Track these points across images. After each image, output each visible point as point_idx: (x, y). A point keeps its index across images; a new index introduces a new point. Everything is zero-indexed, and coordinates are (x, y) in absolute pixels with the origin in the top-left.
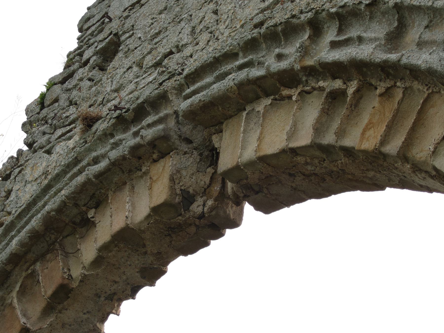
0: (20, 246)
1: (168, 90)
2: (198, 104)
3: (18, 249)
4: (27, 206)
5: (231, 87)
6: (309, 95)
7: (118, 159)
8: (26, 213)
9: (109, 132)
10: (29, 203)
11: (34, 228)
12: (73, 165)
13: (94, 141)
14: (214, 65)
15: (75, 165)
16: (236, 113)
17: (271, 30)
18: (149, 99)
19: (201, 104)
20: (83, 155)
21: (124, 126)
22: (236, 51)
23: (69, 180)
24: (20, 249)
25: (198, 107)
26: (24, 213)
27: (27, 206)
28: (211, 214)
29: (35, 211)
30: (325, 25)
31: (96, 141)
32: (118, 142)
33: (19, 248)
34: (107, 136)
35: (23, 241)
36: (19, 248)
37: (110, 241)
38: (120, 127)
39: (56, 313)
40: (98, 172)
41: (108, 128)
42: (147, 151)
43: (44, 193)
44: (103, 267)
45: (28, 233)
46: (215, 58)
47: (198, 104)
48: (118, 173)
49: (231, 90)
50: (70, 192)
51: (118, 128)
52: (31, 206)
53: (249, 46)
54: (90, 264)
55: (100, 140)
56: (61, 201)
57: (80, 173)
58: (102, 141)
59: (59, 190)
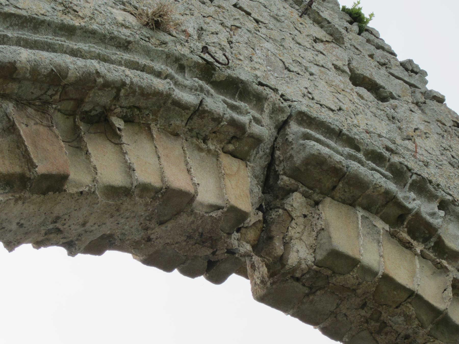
0: (31, 68)
1: (269, 100)
2: (335, 162)
3: (26, 68)
4: (28, 17)
5: (381, 186)
6: (422, 259)
7: (213, 113)
8: (17, 23)
9: (185, 64)
10: (34, 18)
11: (68, 71)
12: (116, 43)
13: (162, 51)
14: (331, 134)
15: (118, 46)
16: (340, 200)
17: (403, 168)
18: (248, 86)
19: (339, 166)
20: (136, 49)
21: (200, 75)
22: (361, 147)
23: (125, 61)
24: (27, 70)
25: (333, 164)
26: (16, 19)
27: (28, 17)
28: (240, 258)
29: (59, 44)
30: (448, 215)
31: (163, 54)
32: (205, 91)
33: (29, 69)
34: (176, 63)
35: (41, 67)
36: (29, 69)
37: (157, 188)
38: (197, 71)
39: (12, 196)
40: (178, 98)
41: (190, 60)
42: (227, 133)
43: (57, 29)
44: (111, 202)
45: (55, 67)
46: (341, 131)
47: (335, 162)
48: (183, 119)
49: (378, 188)
50: (139, 83)
51: (194, 70)
52: (31, 23)
53: (370, 155)
54: (106, 185)
55: (166, 57)
56: (122, 80)
57: (142, 69)
58: (166, 60)
59: (106, 57)
